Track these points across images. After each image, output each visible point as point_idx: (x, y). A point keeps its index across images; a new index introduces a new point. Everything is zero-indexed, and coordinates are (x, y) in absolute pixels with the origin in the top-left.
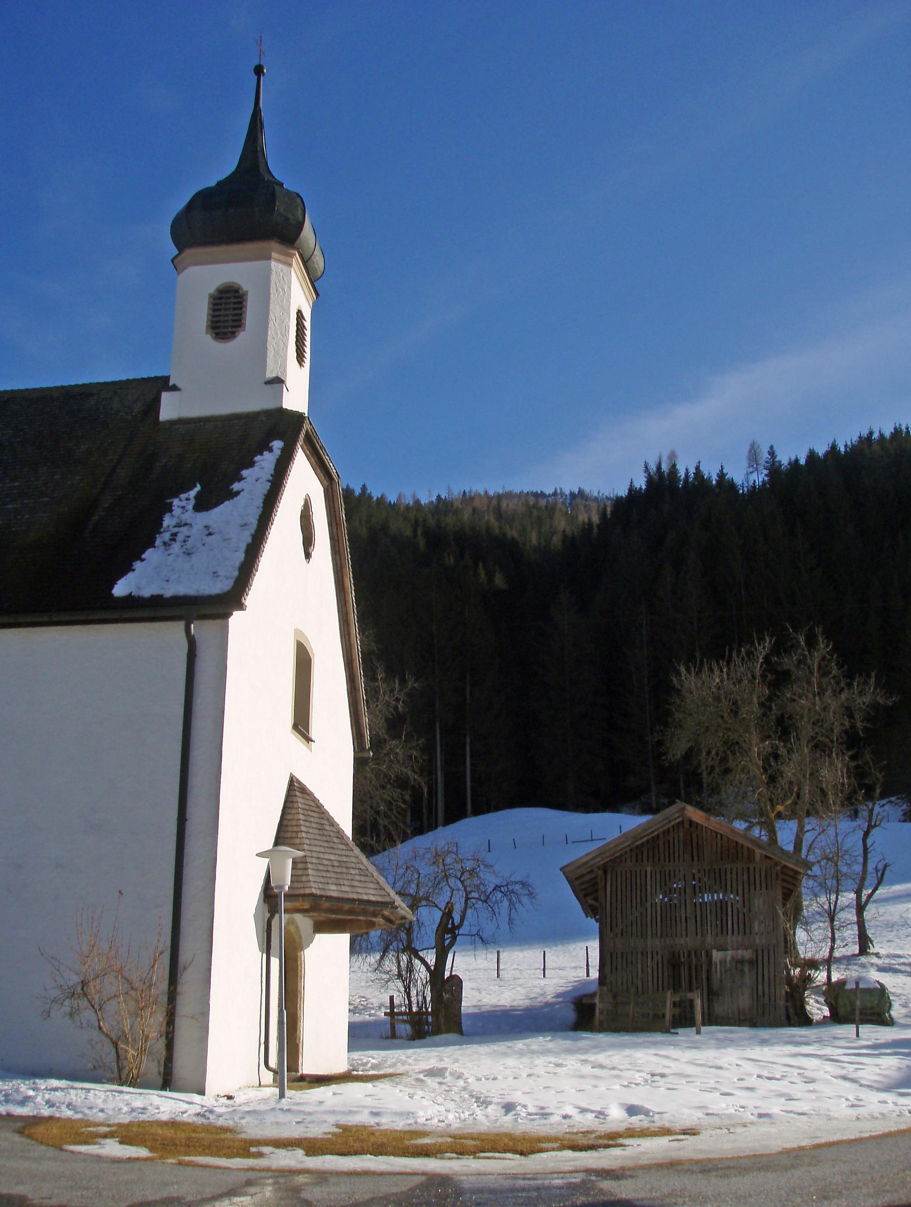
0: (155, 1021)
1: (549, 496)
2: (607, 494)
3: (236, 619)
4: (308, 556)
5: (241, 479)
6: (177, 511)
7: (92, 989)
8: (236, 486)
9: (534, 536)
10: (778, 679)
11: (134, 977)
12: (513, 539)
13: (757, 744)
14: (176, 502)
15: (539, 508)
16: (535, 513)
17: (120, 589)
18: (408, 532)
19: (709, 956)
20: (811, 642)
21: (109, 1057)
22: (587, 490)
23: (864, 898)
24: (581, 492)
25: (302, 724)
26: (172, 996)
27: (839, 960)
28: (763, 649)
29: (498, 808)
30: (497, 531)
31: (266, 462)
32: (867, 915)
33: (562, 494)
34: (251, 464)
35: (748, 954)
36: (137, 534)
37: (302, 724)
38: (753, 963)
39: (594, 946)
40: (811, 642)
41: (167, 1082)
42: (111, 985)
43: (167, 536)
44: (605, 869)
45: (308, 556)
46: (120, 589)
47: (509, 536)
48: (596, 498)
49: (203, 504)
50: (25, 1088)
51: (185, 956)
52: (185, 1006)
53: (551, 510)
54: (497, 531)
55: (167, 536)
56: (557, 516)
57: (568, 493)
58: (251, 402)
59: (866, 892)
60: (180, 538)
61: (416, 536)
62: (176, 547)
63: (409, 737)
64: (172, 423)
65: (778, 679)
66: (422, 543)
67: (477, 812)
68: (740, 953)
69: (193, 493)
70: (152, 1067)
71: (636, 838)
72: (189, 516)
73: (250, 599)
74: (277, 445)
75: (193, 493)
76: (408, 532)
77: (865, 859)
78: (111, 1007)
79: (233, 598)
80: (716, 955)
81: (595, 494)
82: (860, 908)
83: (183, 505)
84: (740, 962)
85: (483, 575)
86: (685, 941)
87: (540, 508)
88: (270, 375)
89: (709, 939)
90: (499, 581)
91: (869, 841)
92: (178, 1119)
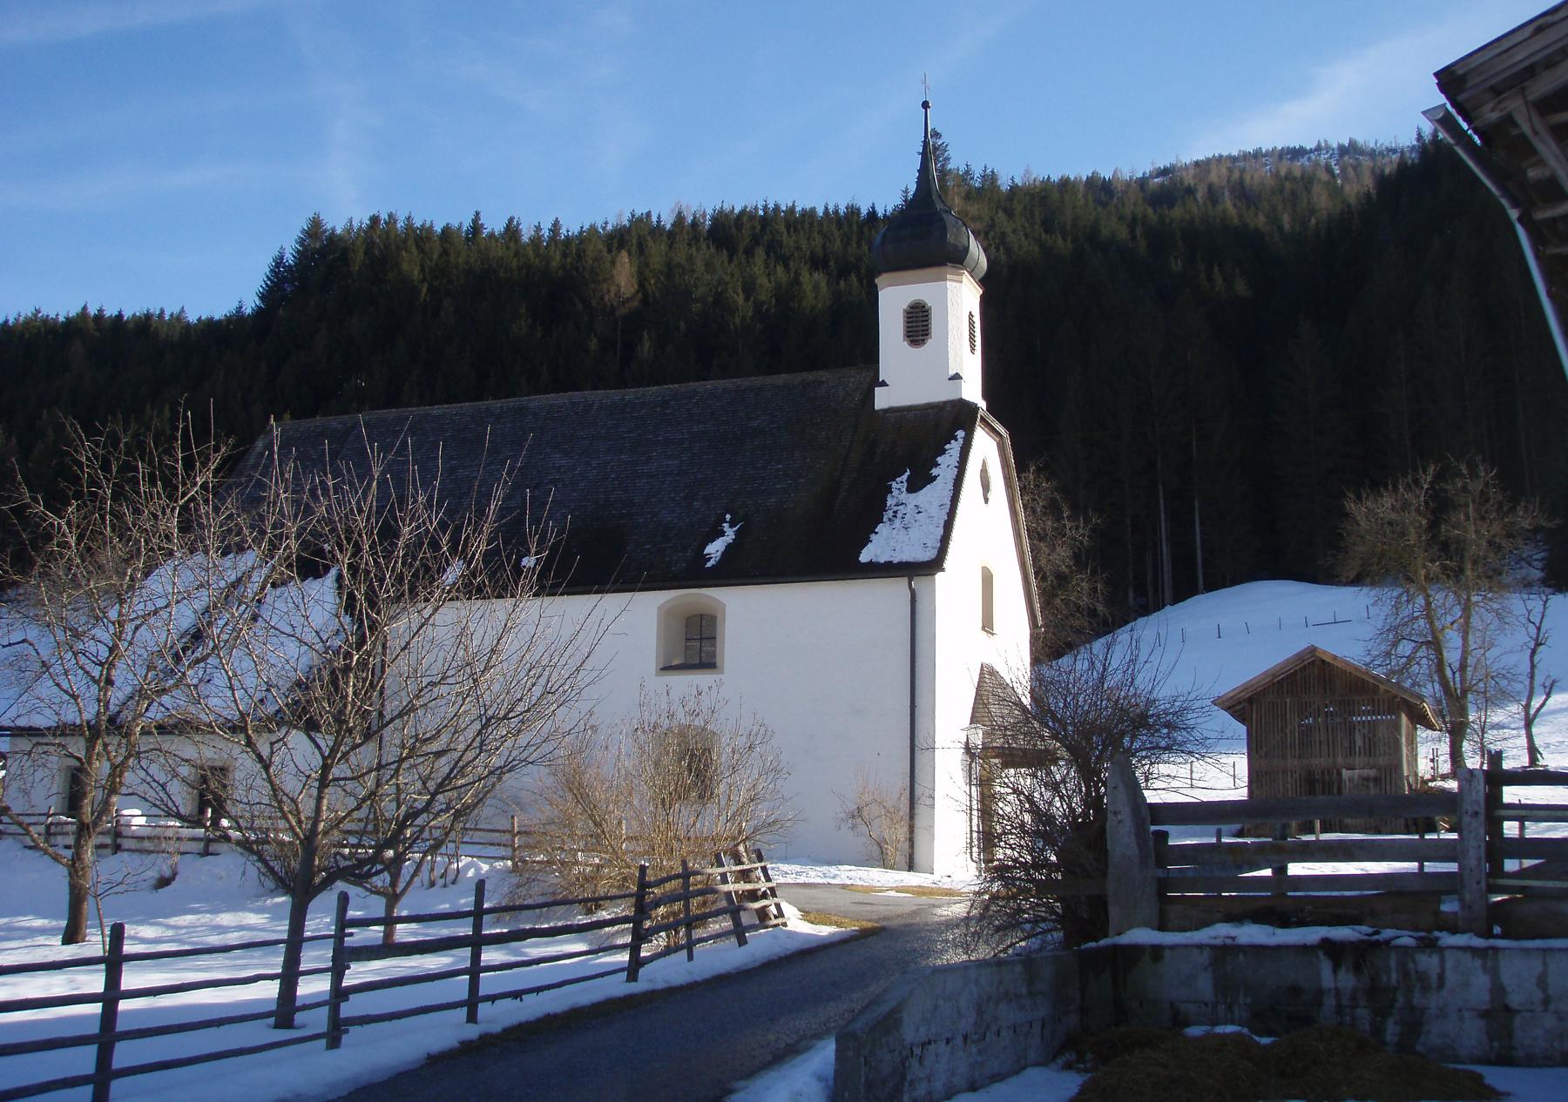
0: (902, 832)
1: (1311, 151)
2: (1387, 144)
3: (939, 576)
4: (986, 500)
5: (937, 465)
6: (895, 493)
7: (865, 812)
8: (934, 472)
9: (1286, 219)
10: (1440, 507)
11: (889, 804)
12: (1257, 230)
13: (1424, 566)
14: (894, 485)
15: (1292, 175)
16: (1288, 185)
17: (865, 557)
18: (1123, 234)
19: (1339, 774)
20: (1472, 468)
21: (876, 851)
22: (1360, 140)
23: (1532, 712)
24: (1352, 143)
25: (987, 625)
26: (912, 817)
27: (677, 876)
28: (1426, 480)
29: (1235, 582)
30: (1236, 221)
31: (954, 448)
32: (1534, 730)
33: (1328, 148)
34: (943, 452)
35: (1372, 773)
36: (871, 514)
37: (987, 625)
38: (1377, 780)
39: (1242, 764)
40: (1472, 468)
41: (911, 867)
42: (875, 810)
43: (890, 513)
44: (1250, 700)
45: (986, 500)
46: (865, 557)
47: (1252, 226)
48: (1373, 150)
49: (914, 487)
50: (833, 870)
51: (919, 791)
52: (920, 822)
53: (1307, 181)
54: (1236, 221)
55: (890, 513)
56: (1316, 189)
57: (1335, 145)
58: (938, 394)
59: (1535, 704)
60: (899, 515)
61: (1134, 238)
62: (897, 522)
63: (1094, 572)
64: (885, 411)
65: (1440, 507)
66: (1142, 244)
67: (1212, 586)
68: (1366, 772)
69: (905, 477)
70: (901, 859)
71: (1275, 676)
72: (904, 497)
73: (949, 563)
74: (960, 434)
75: (905, 477)
76: (1123, 234)
77: (1532, 677)
78: (876, 823)
79: (935, 565)
80: (1346, 773)
81: (1372, 145)
82: (1529, 724)
83: (899, 485)
84: (1367, 779)
85: (1219, 280)
86: (1319, 762)
87: (1295, 178)
88: (952, 373)
89: (1340, 760)
90: (1241, 288)
91: (1536, 658)
92: (1109, 638)
